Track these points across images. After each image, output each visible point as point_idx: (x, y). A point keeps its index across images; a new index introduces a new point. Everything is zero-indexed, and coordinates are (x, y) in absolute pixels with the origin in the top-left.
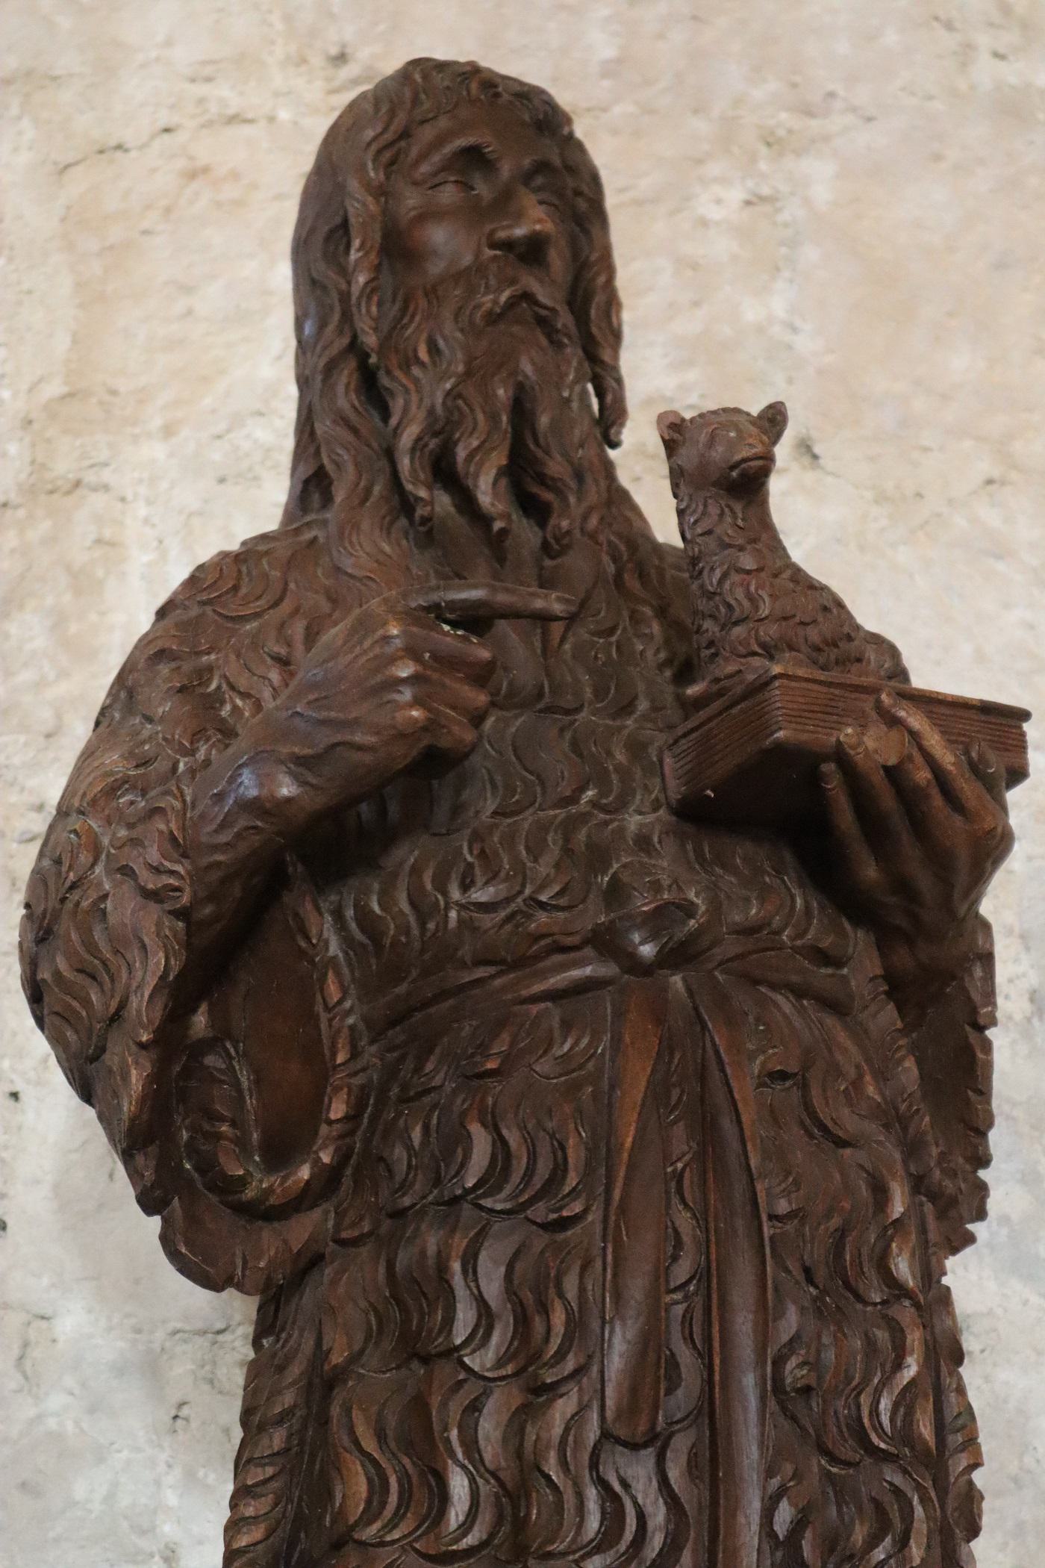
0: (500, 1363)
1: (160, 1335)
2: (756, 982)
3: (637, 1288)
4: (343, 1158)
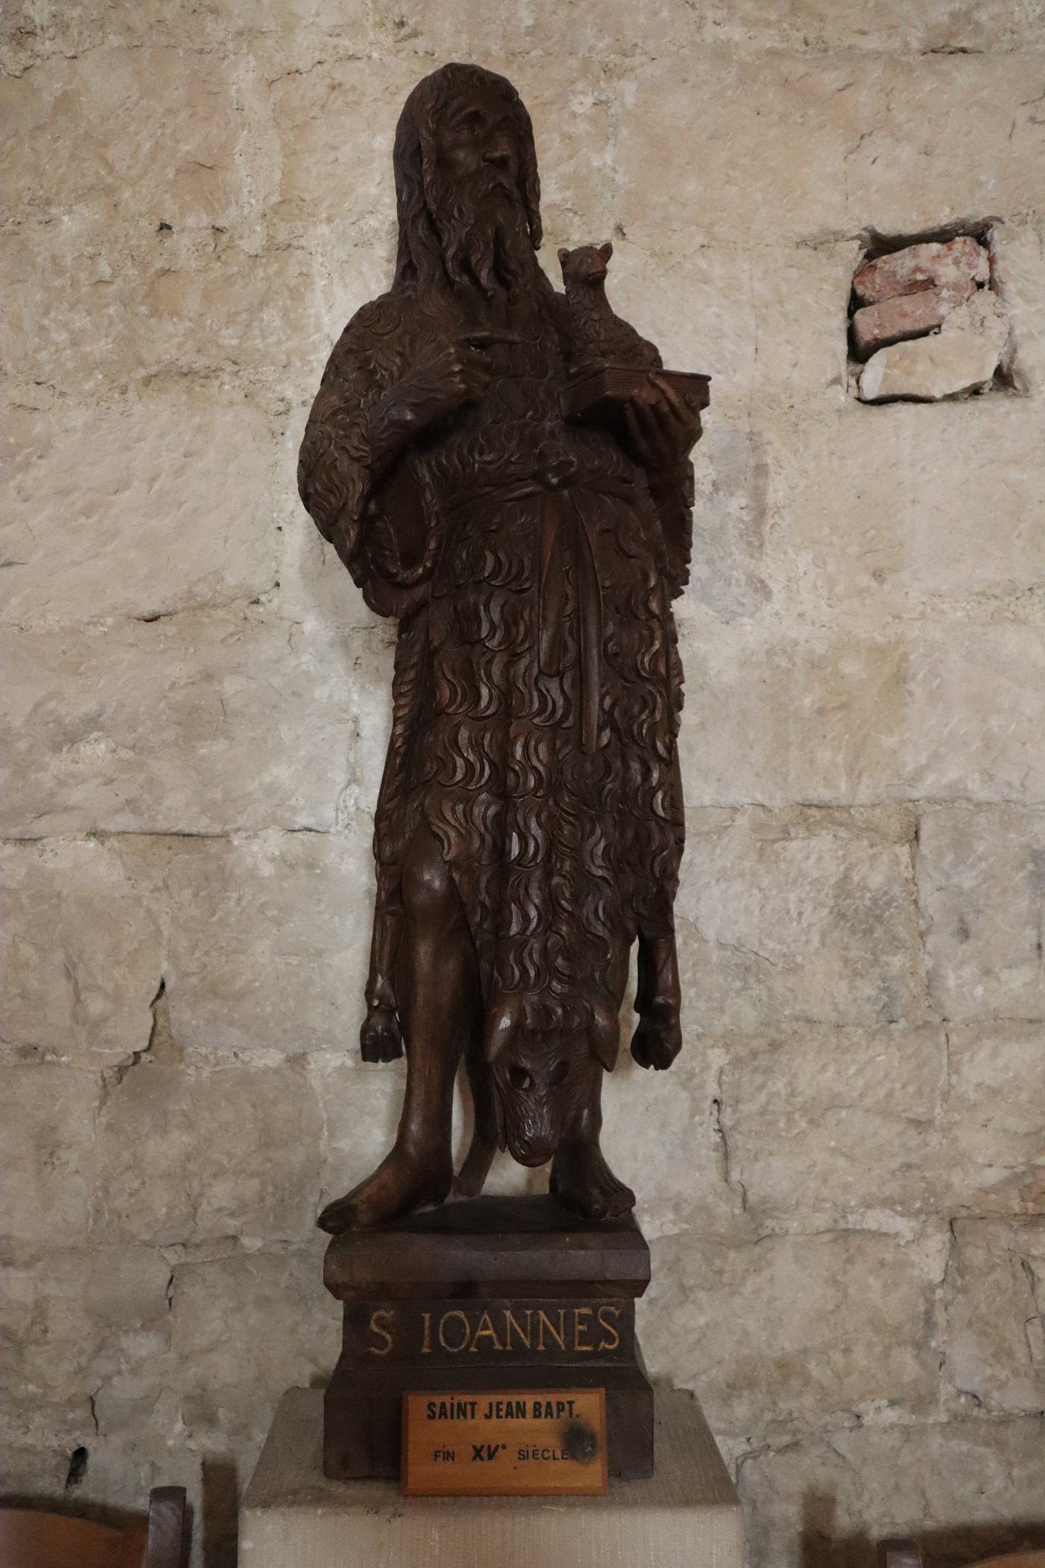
0: (500, 645)
1: (347, 630)
3: (552, 617)
4: (435, 563)
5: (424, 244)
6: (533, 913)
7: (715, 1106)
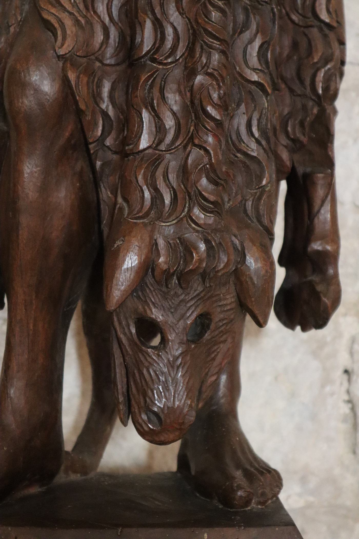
6: (169, 122)
7: (345, 377)
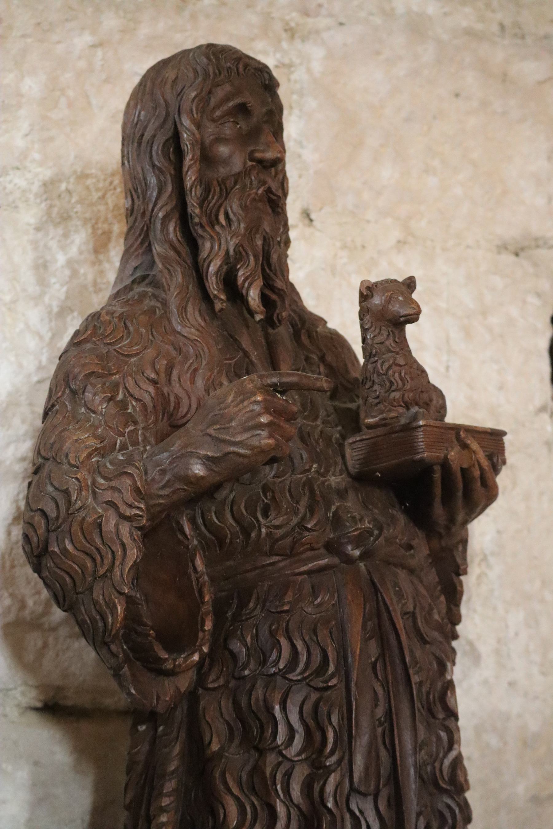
0: (299, 754)
2: (389, 564)
4: (211, 649)
5: (174, 249)
